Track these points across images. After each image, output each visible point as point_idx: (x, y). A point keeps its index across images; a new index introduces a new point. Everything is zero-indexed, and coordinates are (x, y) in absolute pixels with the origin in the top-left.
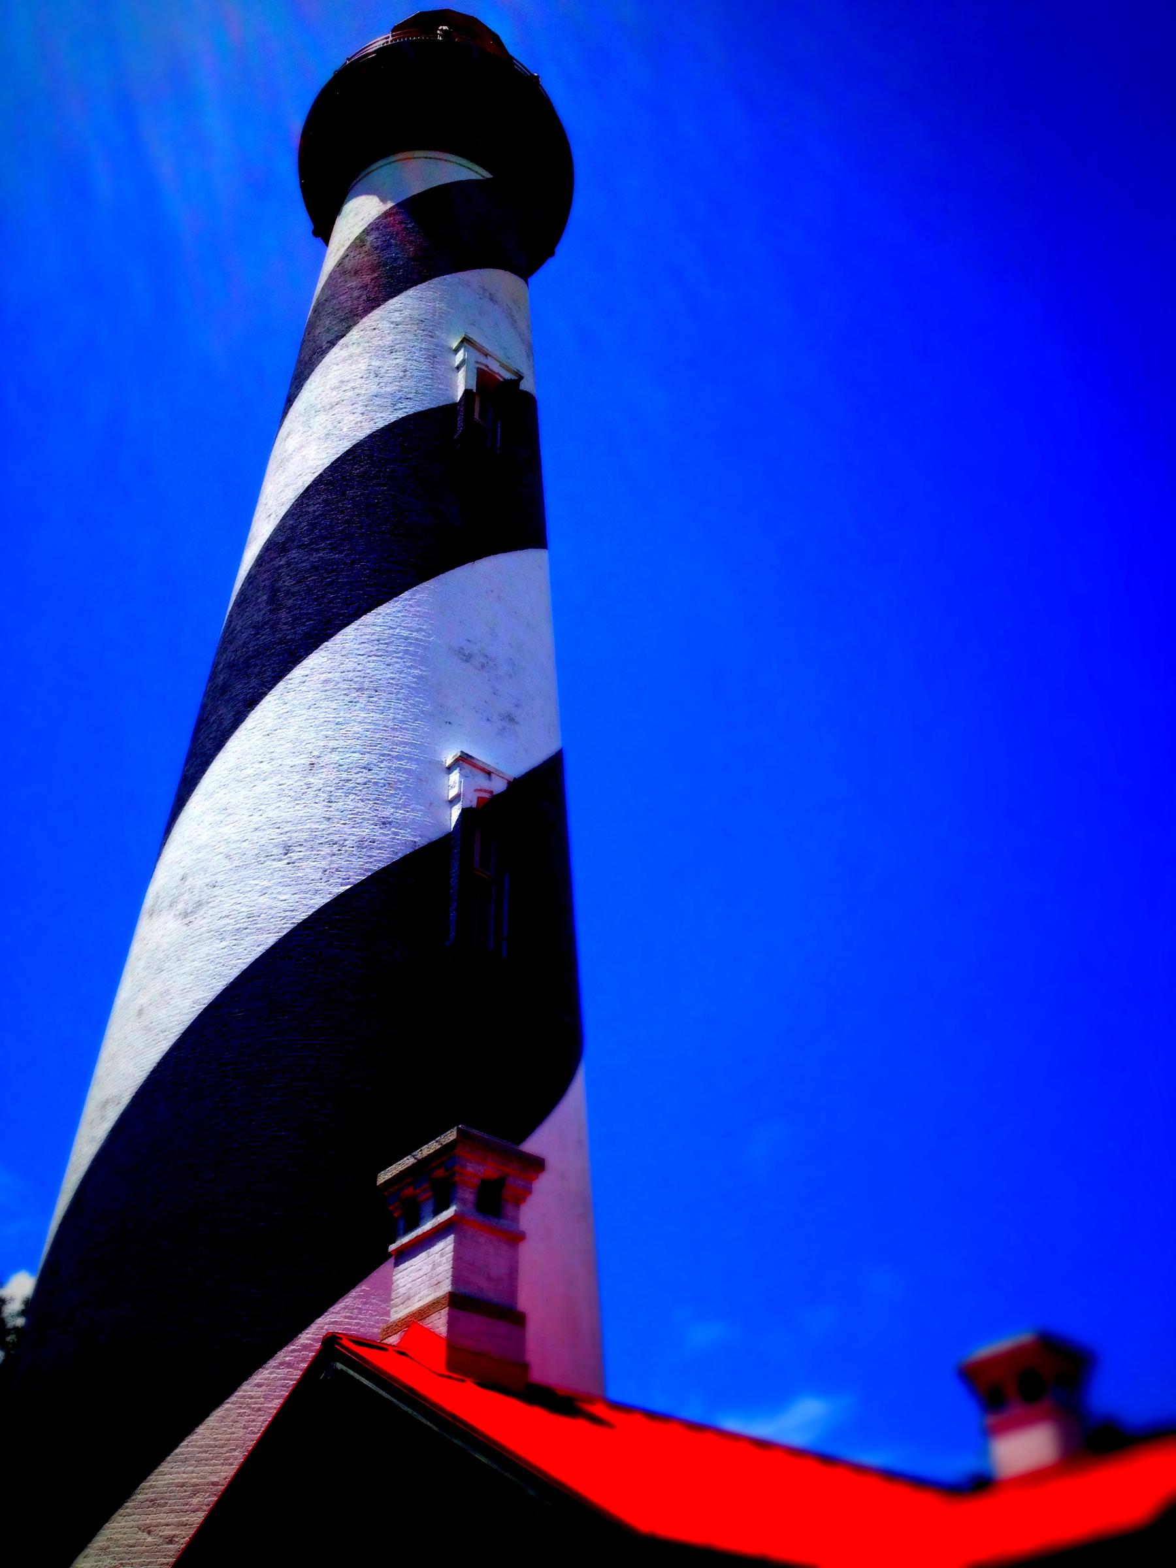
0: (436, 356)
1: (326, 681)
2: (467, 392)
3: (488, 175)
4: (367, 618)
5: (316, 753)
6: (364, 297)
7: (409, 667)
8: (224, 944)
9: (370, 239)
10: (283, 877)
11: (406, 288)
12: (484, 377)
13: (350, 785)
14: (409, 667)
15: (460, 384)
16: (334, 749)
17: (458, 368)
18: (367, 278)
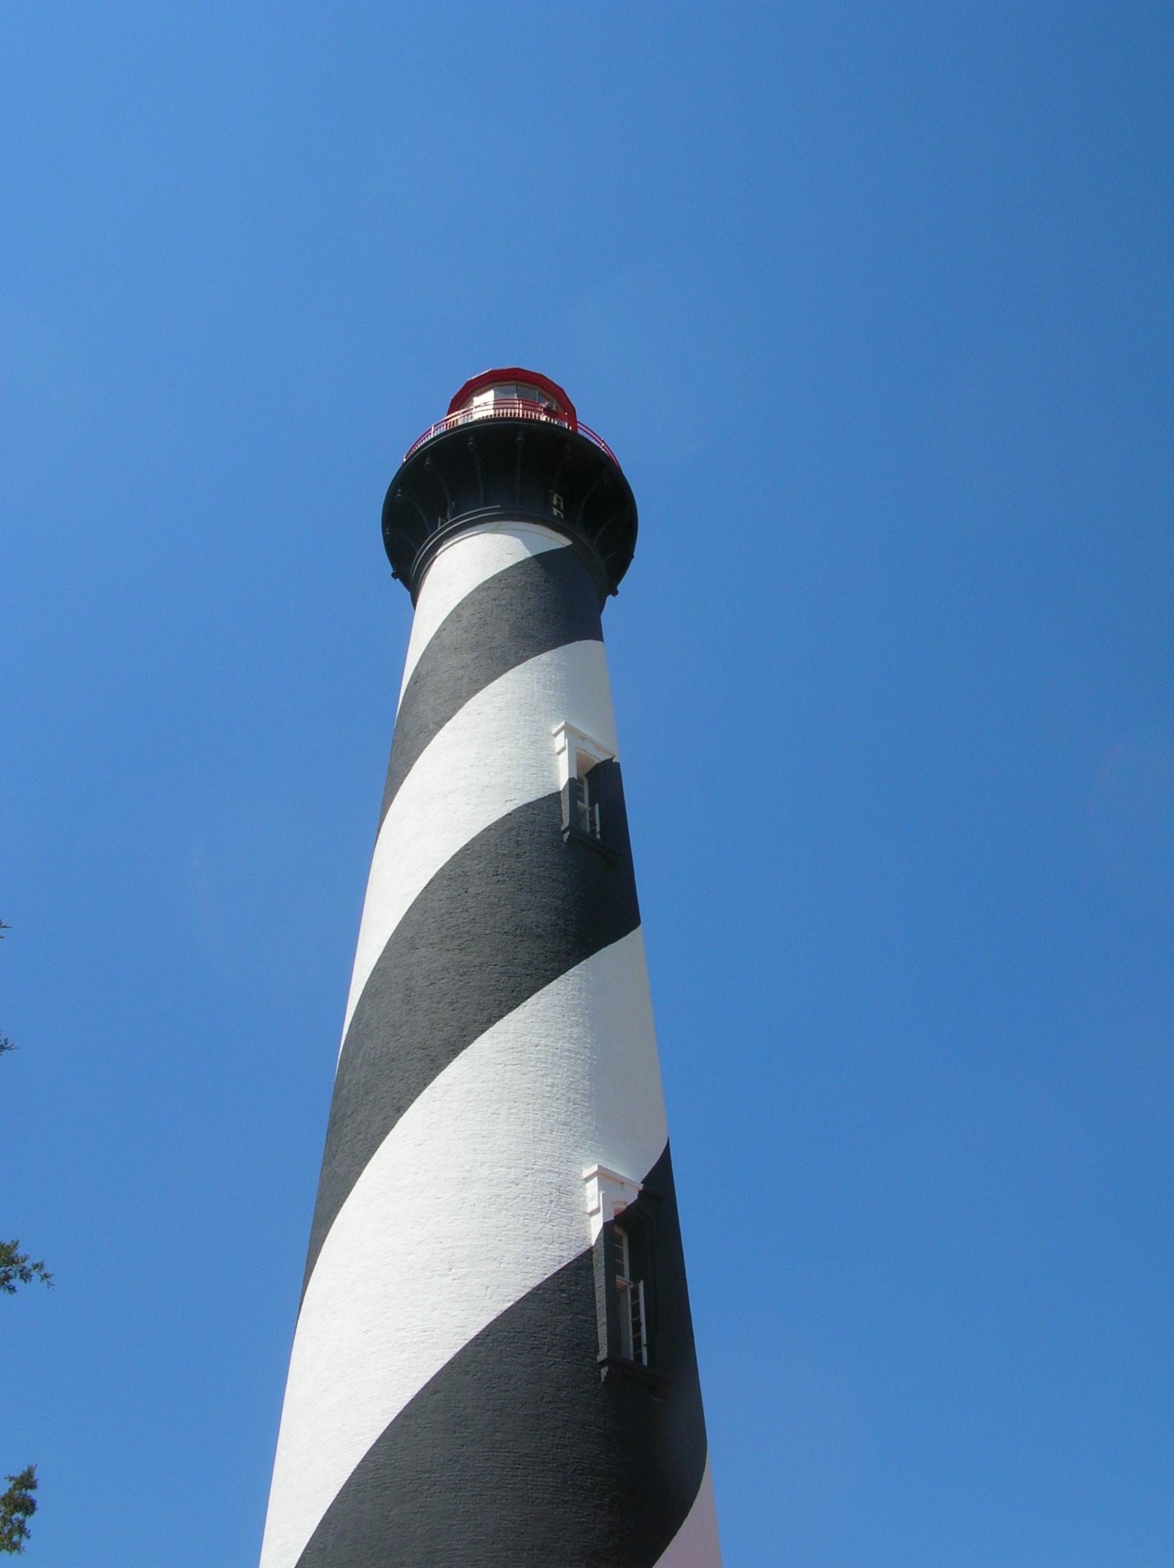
0: (539, 740)
1: (469, 1091)
2: (571, 780)
3: (556, 541)
4: (500, 1025)
5: (467, 1167)
6: (466, 680)
7: (542, 1076)
8: (404, 1356)
9: (466, 614)
10: (451, 1293)
11: (506, 671)
12: (578, 760)
13: (501, 1200)
14: (542, 1076)
15: (562, 775)
16: (483, 1164)
17: (591, 1214)
18: (469, 657)
